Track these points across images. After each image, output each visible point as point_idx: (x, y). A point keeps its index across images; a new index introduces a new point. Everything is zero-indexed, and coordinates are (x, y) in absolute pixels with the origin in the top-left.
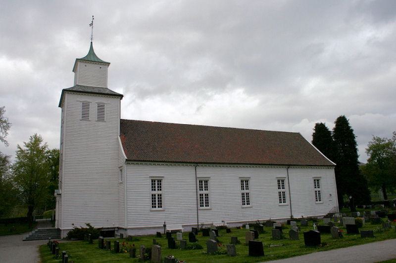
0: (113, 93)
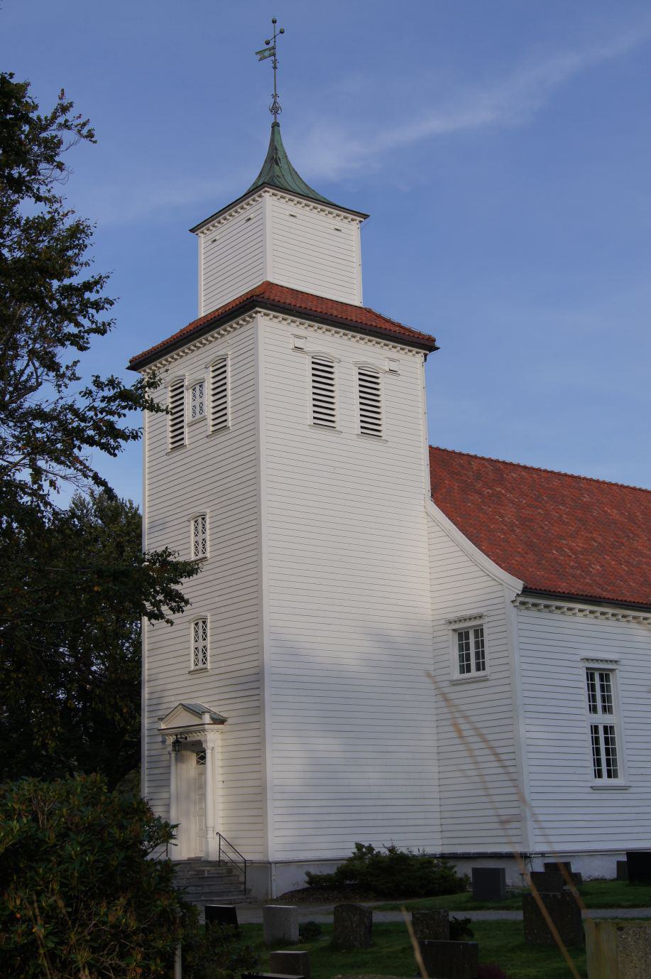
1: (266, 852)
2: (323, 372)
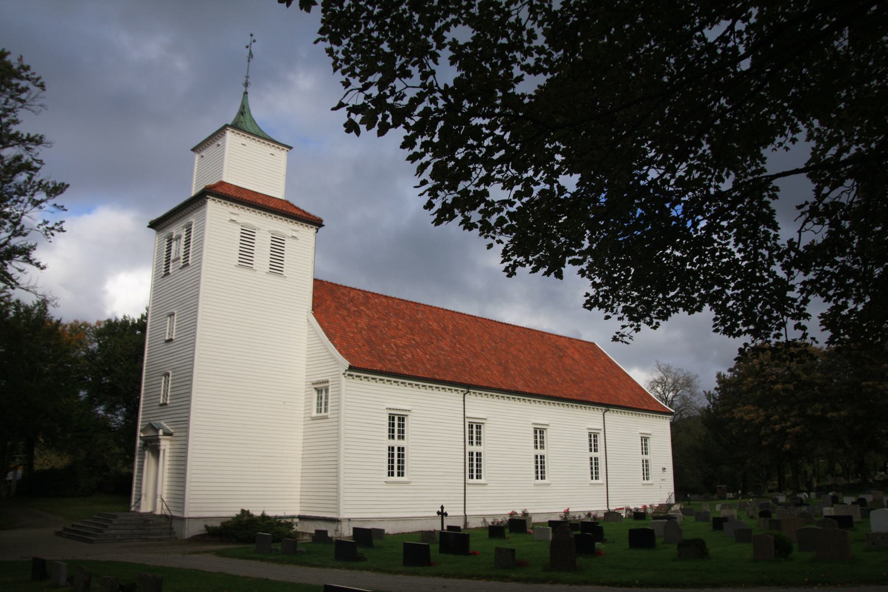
0: (299, 213)
1: (338, 512)
2: (248, 236)
